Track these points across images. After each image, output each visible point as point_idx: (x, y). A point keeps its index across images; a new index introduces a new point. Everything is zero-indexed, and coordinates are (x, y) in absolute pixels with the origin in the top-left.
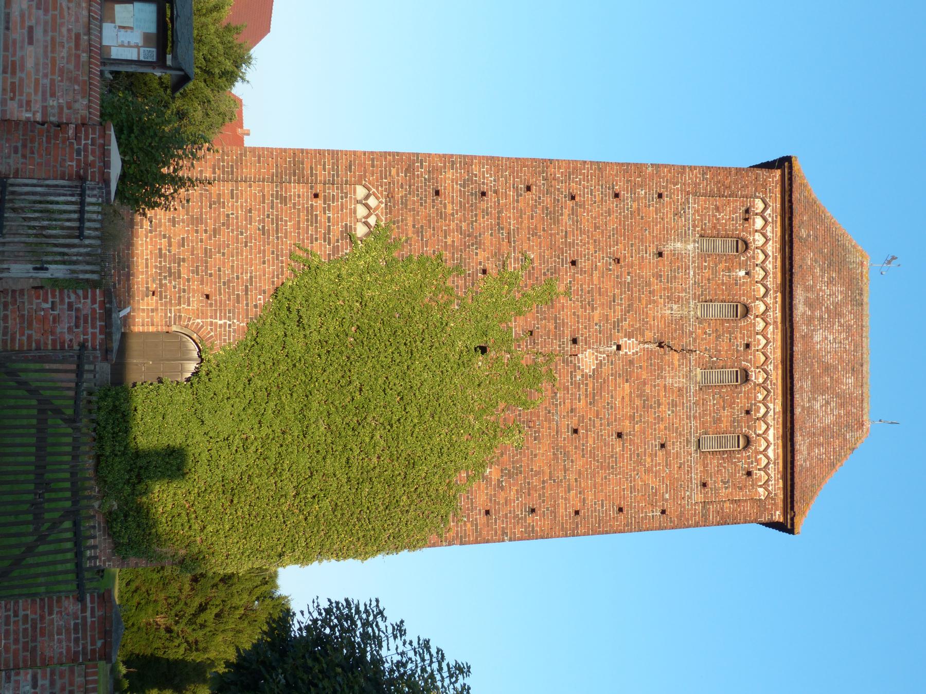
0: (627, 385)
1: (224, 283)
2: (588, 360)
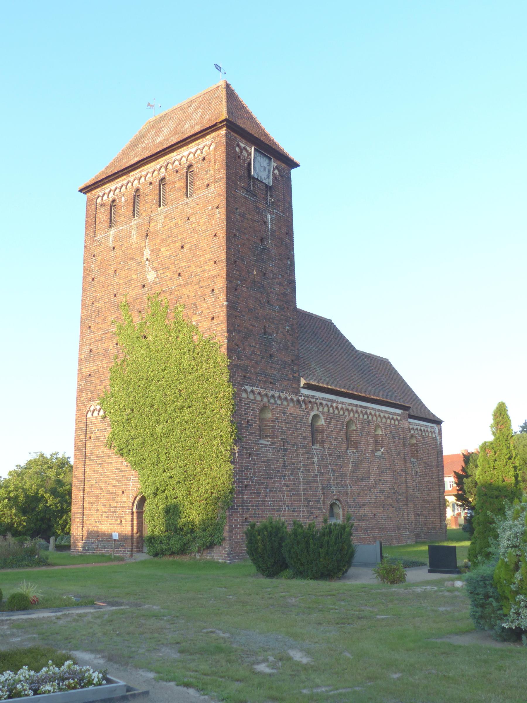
0: (162, 250)
1: (119, 483)
2: (151, 276)
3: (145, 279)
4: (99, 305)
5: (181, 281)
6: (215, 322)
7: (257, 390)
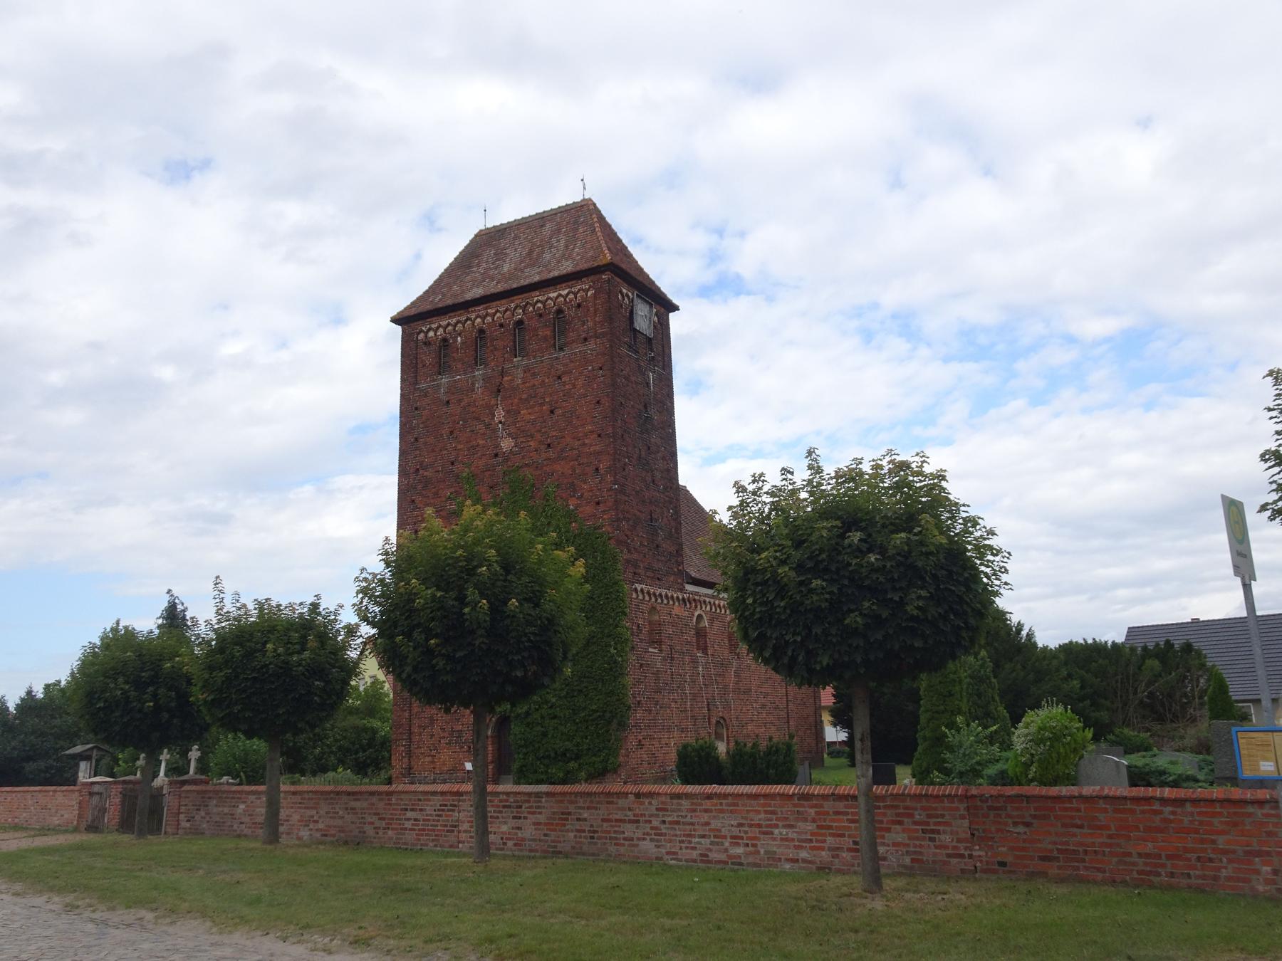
2: (507, 444)
3: (498, 446)
5: (551, 454)
6: (601, 508)
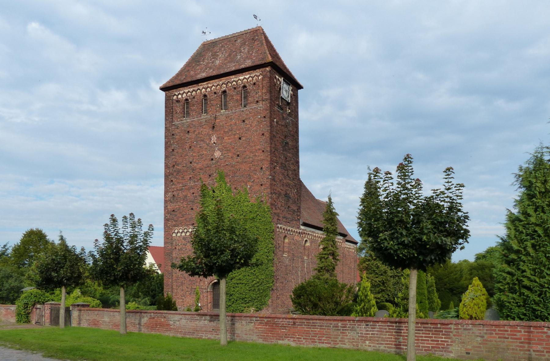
2: (217, 154)
3: (213, 155)
4: (178, 167)
5: (239, 159)
6: (263, 187)
7: (283, 227)
